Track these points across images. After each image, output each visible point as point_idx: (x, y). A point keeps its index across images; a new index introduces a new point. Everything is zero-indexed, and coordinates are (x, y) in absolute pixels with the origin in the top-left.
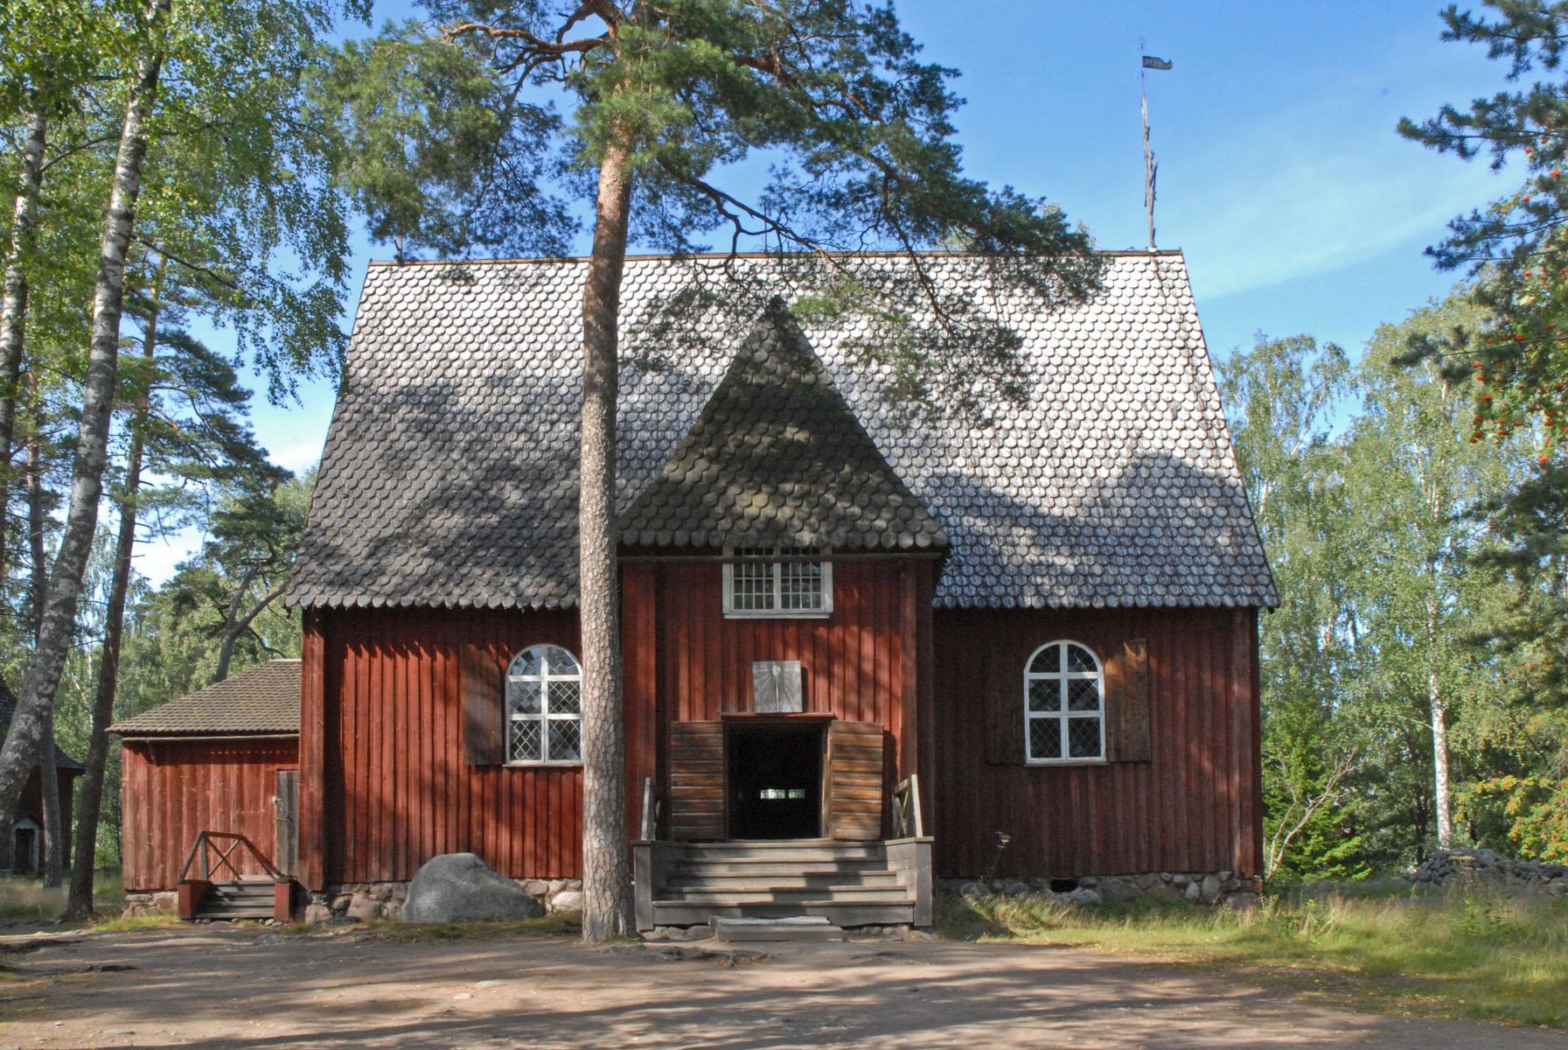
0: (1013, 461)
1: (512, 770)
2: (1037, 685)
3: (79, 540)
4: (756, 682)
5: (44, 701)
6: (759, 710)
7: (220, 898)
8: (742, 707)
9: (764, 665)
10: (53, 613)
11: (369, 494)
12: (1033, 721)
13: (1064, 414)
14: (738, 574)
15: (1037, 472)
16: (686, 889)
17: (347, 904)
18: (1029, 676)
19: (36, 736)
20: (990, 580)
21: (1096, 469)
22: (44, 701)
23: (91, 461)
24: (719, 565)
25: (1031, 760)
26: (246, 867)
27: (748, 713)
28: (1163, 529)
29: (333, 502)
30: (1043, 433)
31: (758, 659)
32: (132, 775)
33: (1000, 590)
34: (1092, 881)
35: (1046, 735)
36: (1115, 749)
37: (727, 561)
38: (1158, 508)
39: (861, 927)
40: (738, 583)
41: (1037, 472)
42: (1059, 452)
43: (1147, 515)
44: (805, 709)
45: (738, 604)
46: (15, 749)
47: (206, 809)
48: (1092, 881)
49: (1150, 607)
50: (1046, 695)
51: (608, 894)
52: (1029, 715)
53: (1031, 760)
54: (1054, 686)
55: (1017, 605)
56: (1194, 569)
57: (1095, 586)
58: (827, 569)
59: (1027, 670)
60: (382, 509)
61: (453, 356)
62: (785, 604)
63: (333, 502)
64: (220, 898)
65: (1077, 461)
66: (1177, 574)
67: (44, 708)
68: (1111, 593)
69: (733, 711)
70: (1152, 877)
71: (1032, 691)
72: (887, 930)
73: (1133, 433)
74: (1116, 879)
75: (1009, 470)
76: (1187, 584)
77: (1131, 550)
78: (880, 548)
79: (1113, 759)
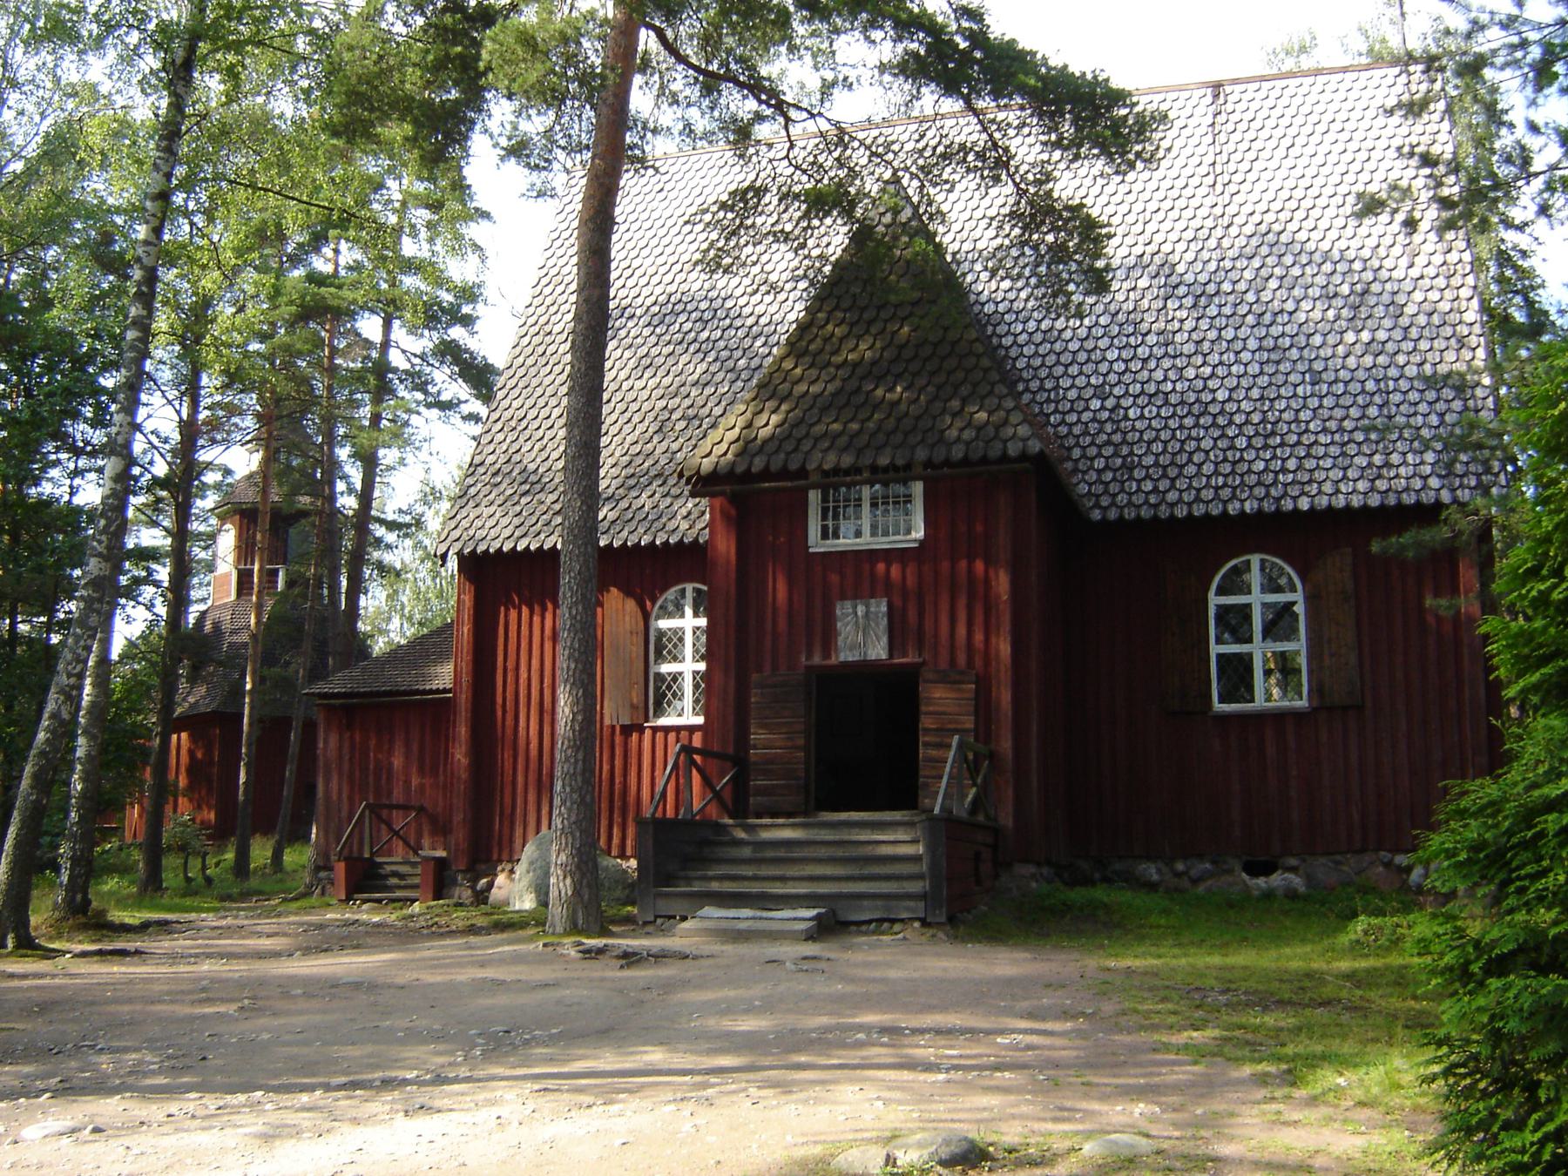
0: (1212, 335)
1: (655, 729)
2: (1223, 611)
3: (107, 519)
4: (839, 624)
5: (73, 680)
6: (842, 659)
7: (386, 877)
8: (827, 655)
9: (848, 604)
10: (84, 593)
11: (536, 424)
12: (1220, 656)
13: (1278, 271)
14: (825, 500)
15: (1238, 345)
16: (692, 874)
17: (490, 885)
18: (1214, 601)
19: (65, 716)
20: (1163, 485)
21: (1309, 336)
22: (73, 680)
23: (120, 440)
24: (803, 493)
25: (1218, 707)
26: (426, 842)
27: (833, 661)
28: (1381, 407)
29: (500, 437)
30: (1251, 297)
31: (843, 598)
32: (326, 742)
33: (1172, 496)
34: (1293, 862)
35: (1238, 673)
36: (1317, 690)
37: (814, 487)
38: (1378, 381)
39: (870, 922)
40: (825, 511)
41: (1238, 345)
42: (1267, 318)
43: (1363, 391)
44: (891, 656)
45: (825, 536)
46: (47, 730)
47: (389, 779)
48: (1293, 862)
49: (1348, 508)
50: (1235, 622)
51: (568, 881)
52: (1215, 649)
53: (1218, 707)
54: (1244, 612)
55: (1278, 509)
56: (1410, 457)
57: (1285, 485)
58: (918, 488)
59: (1211, 594)
60: (545, 441)
61: (636, 264)
62: (873, 534)
63: (500, 437)
64: (386, 877)
65: (1288, 329)
66: (1388, 465)
67: (73, 687)
68: (1303, 493)
69: (817, 660)
70: (1367, 858)
71: (1219, 618)
72: (897, 927)
73: (1358, 288)
74: (1322, 860)
75: (1206, 346)
76: (1397, 476)
77: (1337, 437)
78: (965, 462)
79: (1315, 704)
